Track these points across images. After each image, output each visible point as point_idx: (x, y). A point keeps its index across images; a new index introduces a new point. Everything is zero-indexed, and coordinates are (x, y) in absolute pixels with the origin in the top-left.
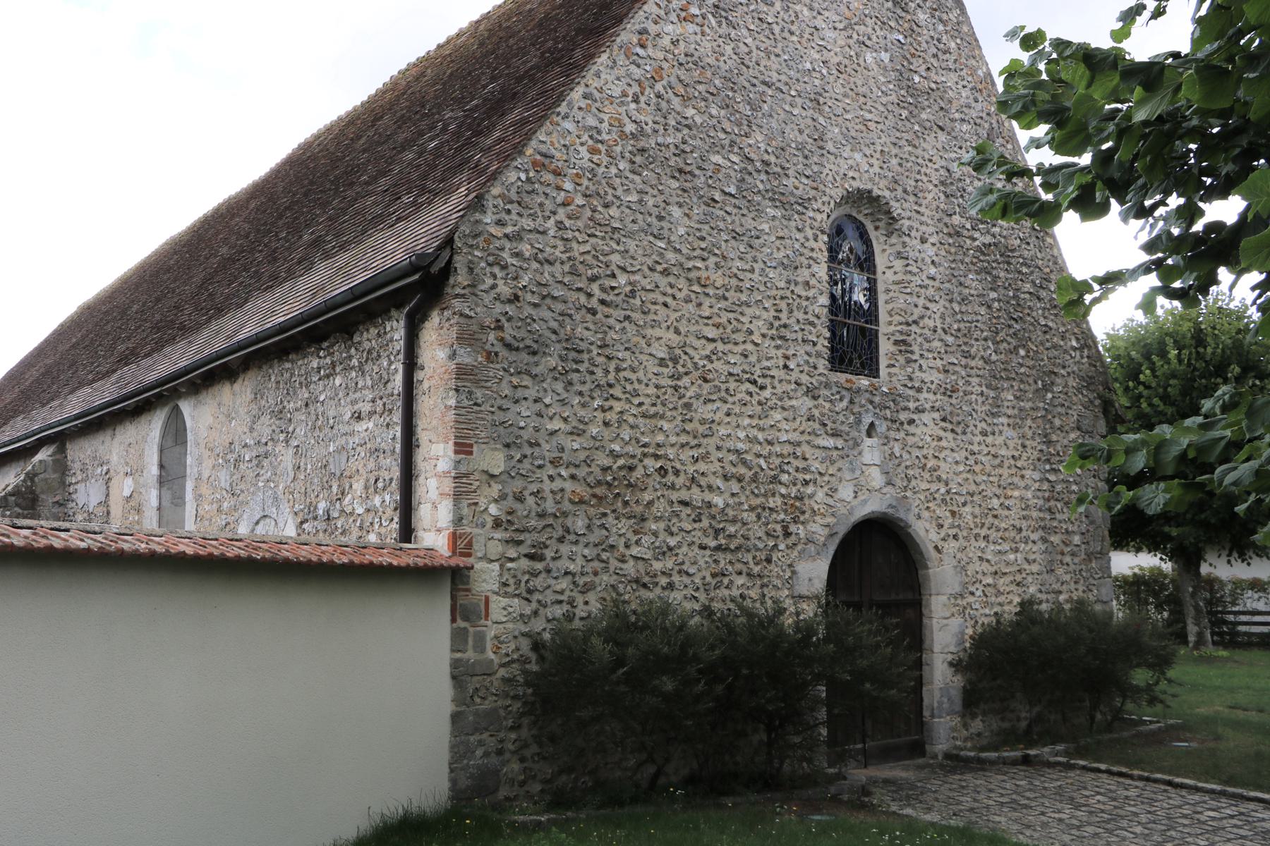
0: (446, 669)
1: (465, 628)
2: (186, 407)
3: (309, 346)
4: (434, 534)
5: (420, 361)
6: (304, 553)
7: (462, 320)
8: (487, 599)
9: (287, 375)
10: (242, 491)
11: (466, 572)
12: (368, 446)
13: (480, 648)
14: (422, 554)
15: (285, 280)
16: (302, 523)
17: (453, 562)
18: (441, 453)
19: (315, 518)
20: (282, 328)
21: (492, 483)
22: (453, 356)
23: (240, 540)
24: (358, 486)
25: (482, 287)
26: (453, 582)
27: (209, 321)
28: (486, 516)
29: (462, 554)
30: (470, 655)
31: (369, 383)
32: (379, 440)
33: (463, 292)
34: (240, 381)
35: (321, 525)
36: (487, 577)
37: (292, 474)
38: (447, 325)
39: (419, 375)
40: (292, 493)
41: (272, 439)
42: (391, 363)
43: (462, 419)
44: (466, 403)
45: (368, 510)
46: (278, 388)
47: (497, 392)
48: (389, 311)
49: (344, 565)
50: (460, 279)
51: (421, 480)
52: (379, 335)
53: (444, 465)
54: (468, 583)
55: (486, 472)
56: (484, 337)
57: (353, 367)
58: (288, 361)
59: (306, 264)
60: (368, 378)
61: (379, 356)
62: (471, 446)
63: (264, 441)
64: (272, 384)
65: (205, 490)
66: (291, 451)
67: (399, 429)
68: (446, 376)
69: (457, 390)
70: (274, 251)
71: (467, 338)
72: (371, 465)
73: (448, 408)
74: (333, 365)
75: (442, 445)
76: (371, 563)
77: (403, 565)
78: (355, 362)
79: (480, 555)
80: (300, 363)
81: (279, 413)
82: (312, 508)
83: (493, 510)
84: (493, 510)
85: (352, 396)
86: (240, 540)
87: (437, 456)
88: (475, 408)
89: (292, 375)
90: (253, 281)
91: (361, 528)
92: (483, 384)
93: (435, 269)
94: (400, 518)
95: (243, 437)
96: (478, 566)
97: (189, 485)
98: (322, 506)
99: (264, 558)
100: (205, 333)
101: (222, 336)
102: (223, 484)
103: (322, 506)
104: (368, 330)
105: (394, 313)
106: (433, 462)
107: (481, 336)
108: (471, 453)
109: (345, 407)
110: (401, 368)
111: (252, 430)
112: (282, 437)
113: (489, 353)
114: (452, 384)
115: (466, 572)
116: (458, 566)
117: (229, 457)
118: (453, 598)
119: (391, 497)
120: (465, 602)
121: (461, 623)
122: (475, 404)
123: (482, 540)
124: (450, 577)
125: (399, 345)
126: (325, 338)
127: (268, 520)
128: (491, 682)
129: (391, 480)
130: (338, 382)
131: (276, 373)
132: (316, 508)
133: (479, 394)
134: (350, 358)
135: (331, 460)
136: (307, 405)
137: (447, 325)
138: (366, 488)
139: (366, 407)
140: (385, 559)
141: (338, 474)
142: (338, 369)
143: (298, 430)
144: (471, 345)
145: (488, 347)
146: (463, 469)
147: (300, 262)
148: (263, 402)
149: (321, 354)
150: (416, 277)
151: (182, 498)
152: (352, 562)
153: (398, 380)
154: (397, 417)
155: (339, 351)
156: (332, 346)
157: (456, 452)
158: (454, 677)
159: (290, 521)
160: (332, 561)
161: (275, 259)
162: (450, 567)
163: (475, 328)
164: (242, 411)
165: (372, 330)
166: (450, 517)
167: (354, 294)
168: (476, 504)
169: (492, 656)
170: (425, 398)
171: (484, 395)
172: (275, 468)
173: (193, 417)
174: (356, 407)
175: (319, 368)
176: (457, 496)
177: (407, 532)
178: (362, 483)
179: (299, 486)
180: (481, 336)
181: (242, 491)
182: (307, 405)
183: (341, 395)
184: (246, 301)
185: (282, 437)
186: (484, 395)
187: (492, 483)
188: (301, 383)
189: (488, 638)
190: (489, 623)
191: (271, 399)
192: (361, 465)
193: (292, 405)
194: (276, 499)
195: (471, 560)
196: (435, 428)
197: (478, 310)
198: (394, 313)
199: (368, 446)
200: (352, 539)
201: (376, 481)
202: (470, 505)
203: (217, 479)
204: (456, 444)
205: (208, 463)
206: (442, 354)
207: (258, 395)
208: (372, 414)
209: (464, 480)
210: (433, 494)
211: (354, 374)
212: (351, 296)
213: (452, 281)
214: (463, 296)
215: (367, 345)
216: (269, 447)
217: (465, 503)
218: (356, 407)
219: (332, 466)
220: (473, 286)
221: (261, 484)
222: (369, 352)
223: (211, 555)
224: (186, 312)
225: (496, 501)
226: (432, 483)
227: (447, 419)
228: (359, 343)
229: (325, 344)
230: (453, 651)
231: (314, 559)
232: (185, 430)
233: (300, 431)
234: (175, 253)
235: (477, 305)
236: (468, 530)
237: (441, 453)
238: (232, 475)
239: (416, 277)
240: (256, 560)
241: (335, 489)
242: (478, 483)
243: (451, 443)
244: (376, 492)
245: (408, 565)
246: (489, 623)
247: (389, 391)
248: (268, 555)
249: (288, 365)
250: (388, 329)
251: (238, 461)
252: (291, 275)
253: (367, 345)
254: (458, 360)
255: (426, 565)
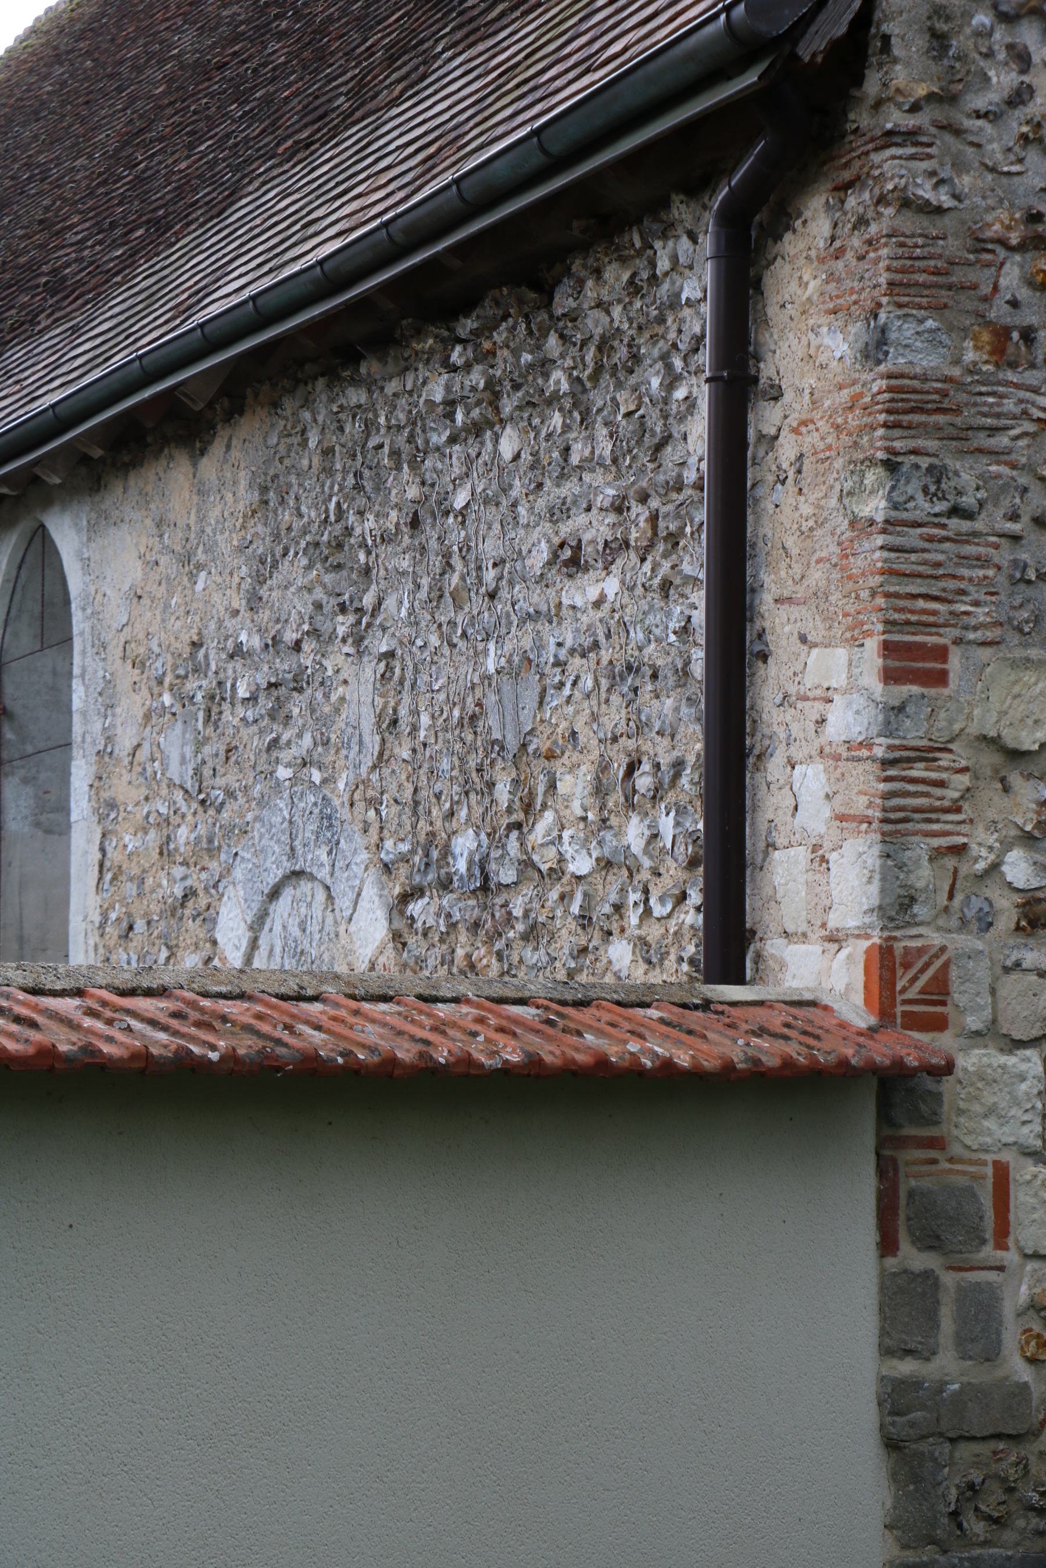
0: (865, 1416)
1: (927, 1275)
2: (66, 533)
3: (419, 333)
4: (818, 959)
5: (767, 371)
6: (372, 1034)
7: (909, 223)
8: (1002, 1172)
9: (354, 429)
10: (230, 794)
11: (929, 1083)
12: (605, 655)
13: (980, 1338)
14: (776, 1020)
15: (348, 119)
16: (405, 898)
17: (883, 1051)
18: (839, 680)
19: (445, 885)
20: (330, 278)
21: (1015, 779)
22: (876, 348)
23: (161, 992)
24: (575, 786)
25: (981, 102)
26: (885, 1116)
27: (128, 262)
28: (993, 891)
29: (913, 1022)
30: (947, 1367)
31: (605, 448)
32: (637, 635)
33: (910, 122)
34: (217, 449)
35: (462, 907)
36: (1001, 1099)
37: (373, 743)
38: (856, 242)
39: (765, 418)
40: (374, 803)
41: (314, 633)
42: (672, 381)
43: (908, 563)
44: (923, 507)
45: (606, 864)
46: (328, 471)
47: (1029, 468)
48: (665, 204)
49: (507, 1071)
50: (900, 76)
51: (775, 768)
52: (634, 288)
53: (848, 720)
54: (934, 1119)
55: (994, 742)
56: (983, 278)
57: (554, 400)
58: (355, 382)
59: (408, 64)
60: (602, 432)
61: (636, 358)
62: (941, 653)
63: (290, 636)
64: (310, 460)
65: (124, 788)
66: (371, 670)
67: (699, 597)
68: (854, 420)
69: (891, 466)
70: (322, 31)
71: (926, 282)
72: (615, 716)
73: (861, 526)
74: (493, 391)
75: (841, 654)
76: (602, 1063)
77: (709, 1064)
78: (559, 380)
79: (974, 1022)
80: (392, 387)
81: (333, 551)
82: (434, 850)
83: (1018, 868)
84: (1018, 868)
85: (553, 493)
86: (161, 992)
87: (826, 688)
88: (954, 523)
89: (370, 427)
90: (257, 129)
91: (585, 920)
92: (982, 440)
93: (812, 46)
94: (706, 891)
95: (230, 623)
96: (969, 1061)
97: (81, 773)
98: (465, 844)
99: (230, 1057)
100: (119, 302)
101: (162, 309)
102: (174, 771)
103: (465, 844)
104: (598, 273)
105: (681, 211)
106: (812, 710)
107: (972, 275)
108: (941, 678)
109: (527, 534)
110: (703, 394)
111: (254, 602)
112: (343, 625)
113: (1002, 334)
114: (876, 443)
115: (929, 1083)
116: (898, 1063)
117: (191, 685)
118: (886, 1171)
119: (669, 828)
120: (926, 1183)
121: (913, 1258)
122: (955, 511)
123: (981, 970)
124: (870, 1101)
125: (699, 320)
126: (466, 306)
127: (305, 886)
128: (1023, 1464)
129: (678, 765)
130: (508, 446)
131: (321, 418)
132: (447, 851)
133: (966, 475)
134: (544, 366)
135: (492, 698)
136: (415, 523)
137: (856, 242)
138: (600, 790)
139: (595, 529)
140: (653, 1048)
141: (512, 743)
142: (507, 406)
143: (390, 602)
144: (938, 308)
145: (1000, 311)
146: (914, 733)
147: (391, 60)
148: (286, 517)
149: (456, 356)
150: (751, 78)
151: (63, 808)
152: (534, 1062)
153: (697, 434)
154: (694, 561)
155: (510, 347)
156: (488, 328)
157: (889, 676)
158: (892, 1444)
159: (370, 892)
160: (468, 1061)
161: (322, 57)
162: (872, 1069)
163: (953, 246)
164: (226, 543)
165: (609, 274)
166: (872, 895)
167: (550, 151)
168: (959, 850)
169: (1024, 1373)
170: (785, 495)
171: (985, 479)
172: (324, 722)
173: (86, 564)
174: (565, 529)
175: (450, 404)
176: (895, 826)
177: (730, 944)
178: (586, 773)
179: (396, 782)
180: (972, 275)
181: (230, 794)
182: (415, 523)
183: (517, 489)
184: (234, 194)
185: (343, 625)
186: (985, 479)
187: (1015, 779)
188: (395, 454)
189: (1008, 1311)
190: (1011, 1257)
191: (307, 510)
192: (583, 715)
193: (370, 522)
194: (328, 820)
195: (945, 1041)
196: (820, 596)
197: (965, 182)
198: (681, 211)
199: (605, 655)
200: (540, 968)
201: (632, 768)
202: (937, 854)
203: (158, 754)
204: (888, 649)
205: (132, 705)
206: (838, 345)
207: (270, 492)
208: (614, 549)
209: (918, 771)
210: (815, 817)
211: (557, 420)
212: (537, 160)
213: (872, 86)
214: (911, 136)
215: (595, 323)
216: (307, 660)
217: (920, 849)
218: (565, 529)
219: (493, 720)
220: (946, 98)
221: (283, 773)
222: (605, 345)
223: (47, 1053)
224: (71, 238)
225: (1028, 839)
226: (812, 780)
227: (857, 564)
228: (573, 317)
229: (467, 325)
230: (887, 1352)
231: (406, 1052)
232: (67, 602)
233: (397, 607)
234: (58, 58)
235: (960, 166)
236: (936, 939)
237: (839, 680)
238: (200, 744)
239: (751, 78)
240: (203, 1063)
241: (503, 792)
242: (965, 780)
243: (872, 645)
244: (630, 805)
245: (729, 1067)
246: (1011, 1257)
247: (669, 472)
248: (246, 1046)
249: (356, 396)
250: (663, 264)
251: (218, 698)
252: (366, 100)
253: (595, 323)
254: (896, 361)
255: (788, 1063)
